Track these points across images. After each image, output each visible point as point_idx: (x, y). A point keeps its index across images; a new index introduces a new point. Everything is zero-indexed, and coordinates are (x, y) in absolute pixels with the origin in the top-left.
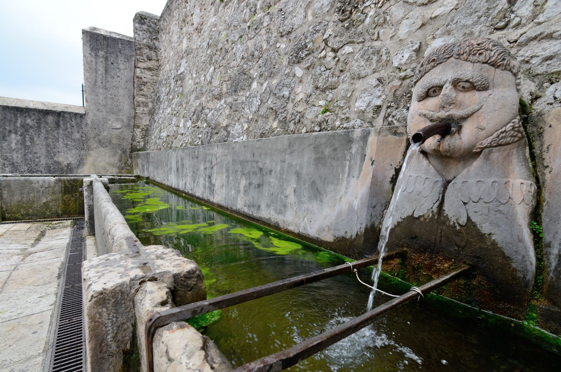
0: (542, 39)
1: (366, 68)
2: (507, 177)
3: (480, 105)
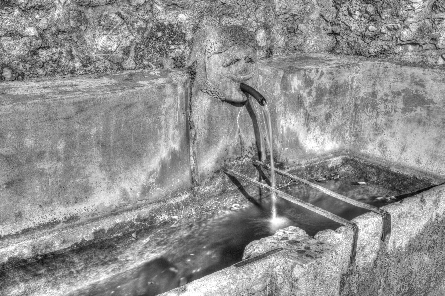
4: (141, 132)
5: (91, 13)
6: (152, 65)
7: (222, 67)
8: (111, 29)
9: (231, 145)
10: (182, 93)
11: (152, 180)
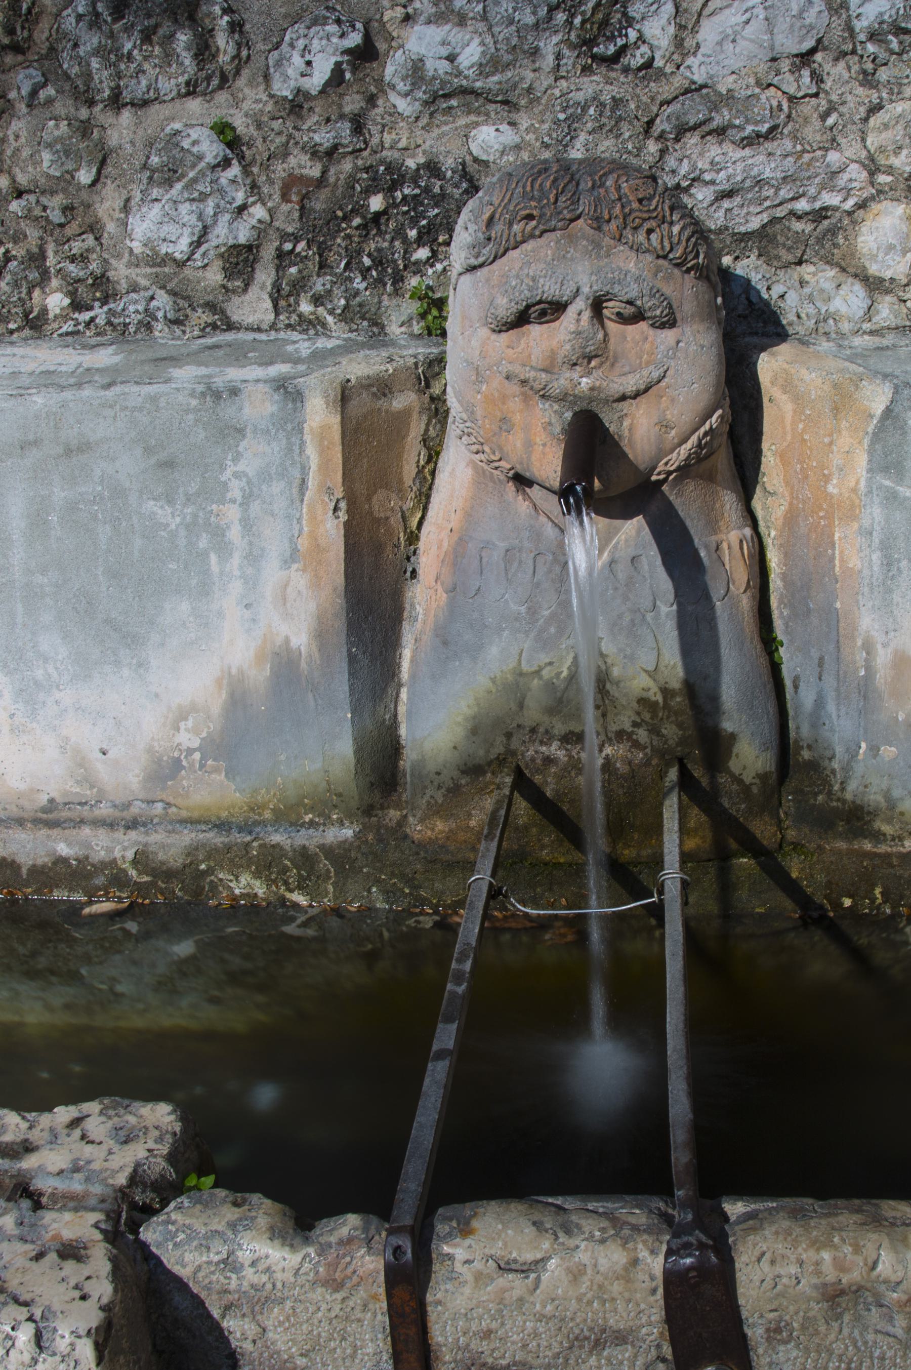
0: (709, 133)
1: (146, 66)
2: (716, 534)
3: (662, 370)
4: (136, 553)
5: (127, 128)
6: (330, 319)
7: (484, 332)
8: (179, 180)
9: (538, 673)
10: (325, 428)
11: (187, 739)
